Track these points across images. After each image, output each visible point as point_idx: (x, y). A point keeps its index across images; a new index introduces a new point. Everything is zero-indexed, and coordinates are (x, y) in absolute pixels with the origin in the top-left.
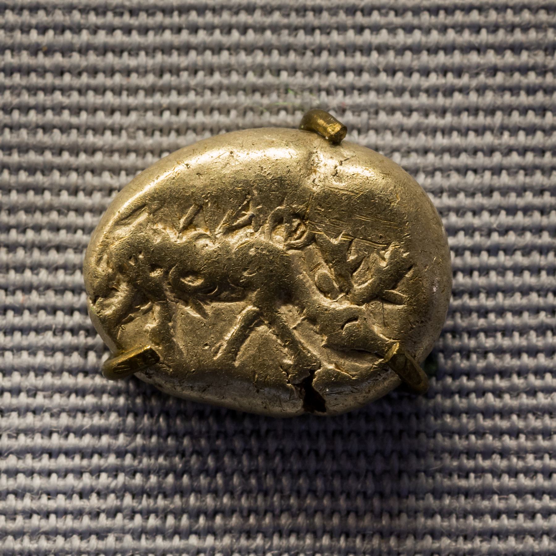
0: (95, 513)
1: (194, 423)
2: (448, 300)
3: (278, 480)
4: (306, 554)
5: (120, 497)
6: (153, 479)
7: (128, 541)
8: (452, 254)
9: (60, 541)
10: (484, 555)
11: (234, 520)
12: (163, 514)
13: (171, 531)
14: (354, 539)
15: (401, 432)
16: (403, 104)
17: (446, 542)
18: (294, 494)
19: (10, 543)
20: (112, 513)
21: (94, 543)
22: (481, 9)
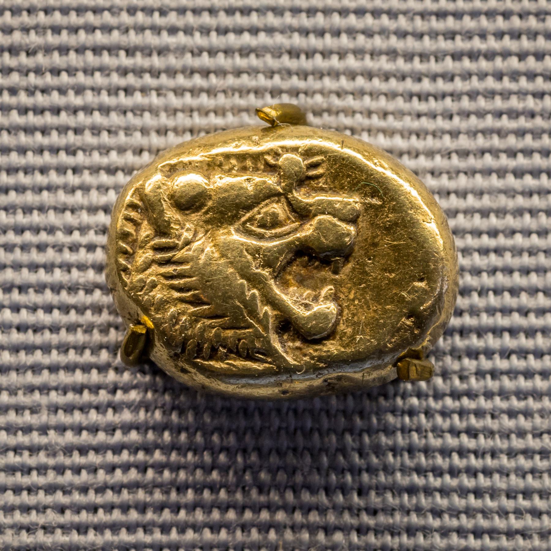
0: (407, 509)
1: (224, 420)
2: (455, 298)
3: (255, 475)
4: (301, 550)
5: (167, 492)
6: (167, 474)
7: (207, 535)
8: (460, 255)
9: (108, 536)
10: (98, 549)
11: (231, 515)
12: (142, 508)
13: (333, 527)
14: (266, 535)
15: (311, 429)
16: (184, 105)
17: (91, 536)
18: (240, 490)
19: (9, 538)
20: (160, 508)
21: (140, 536)
22: (47, 11)
